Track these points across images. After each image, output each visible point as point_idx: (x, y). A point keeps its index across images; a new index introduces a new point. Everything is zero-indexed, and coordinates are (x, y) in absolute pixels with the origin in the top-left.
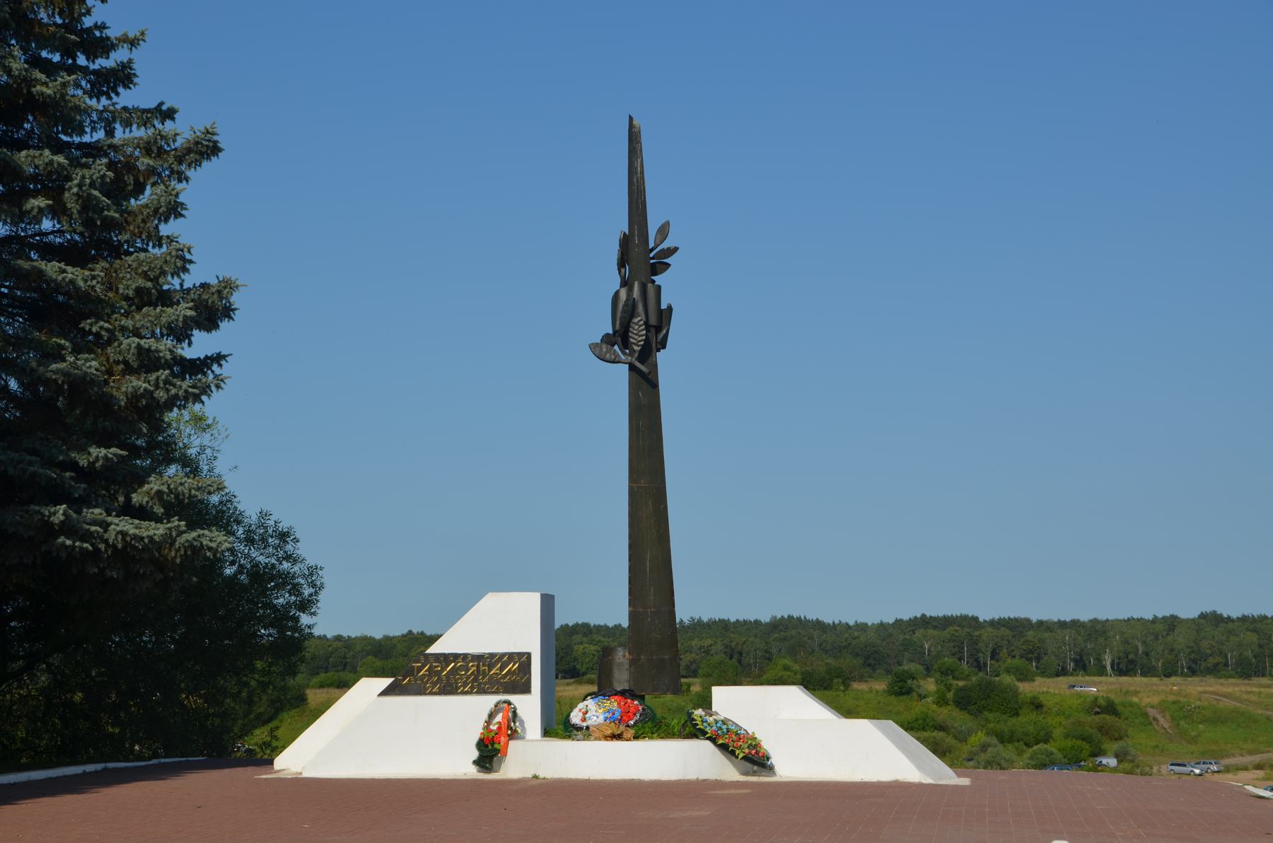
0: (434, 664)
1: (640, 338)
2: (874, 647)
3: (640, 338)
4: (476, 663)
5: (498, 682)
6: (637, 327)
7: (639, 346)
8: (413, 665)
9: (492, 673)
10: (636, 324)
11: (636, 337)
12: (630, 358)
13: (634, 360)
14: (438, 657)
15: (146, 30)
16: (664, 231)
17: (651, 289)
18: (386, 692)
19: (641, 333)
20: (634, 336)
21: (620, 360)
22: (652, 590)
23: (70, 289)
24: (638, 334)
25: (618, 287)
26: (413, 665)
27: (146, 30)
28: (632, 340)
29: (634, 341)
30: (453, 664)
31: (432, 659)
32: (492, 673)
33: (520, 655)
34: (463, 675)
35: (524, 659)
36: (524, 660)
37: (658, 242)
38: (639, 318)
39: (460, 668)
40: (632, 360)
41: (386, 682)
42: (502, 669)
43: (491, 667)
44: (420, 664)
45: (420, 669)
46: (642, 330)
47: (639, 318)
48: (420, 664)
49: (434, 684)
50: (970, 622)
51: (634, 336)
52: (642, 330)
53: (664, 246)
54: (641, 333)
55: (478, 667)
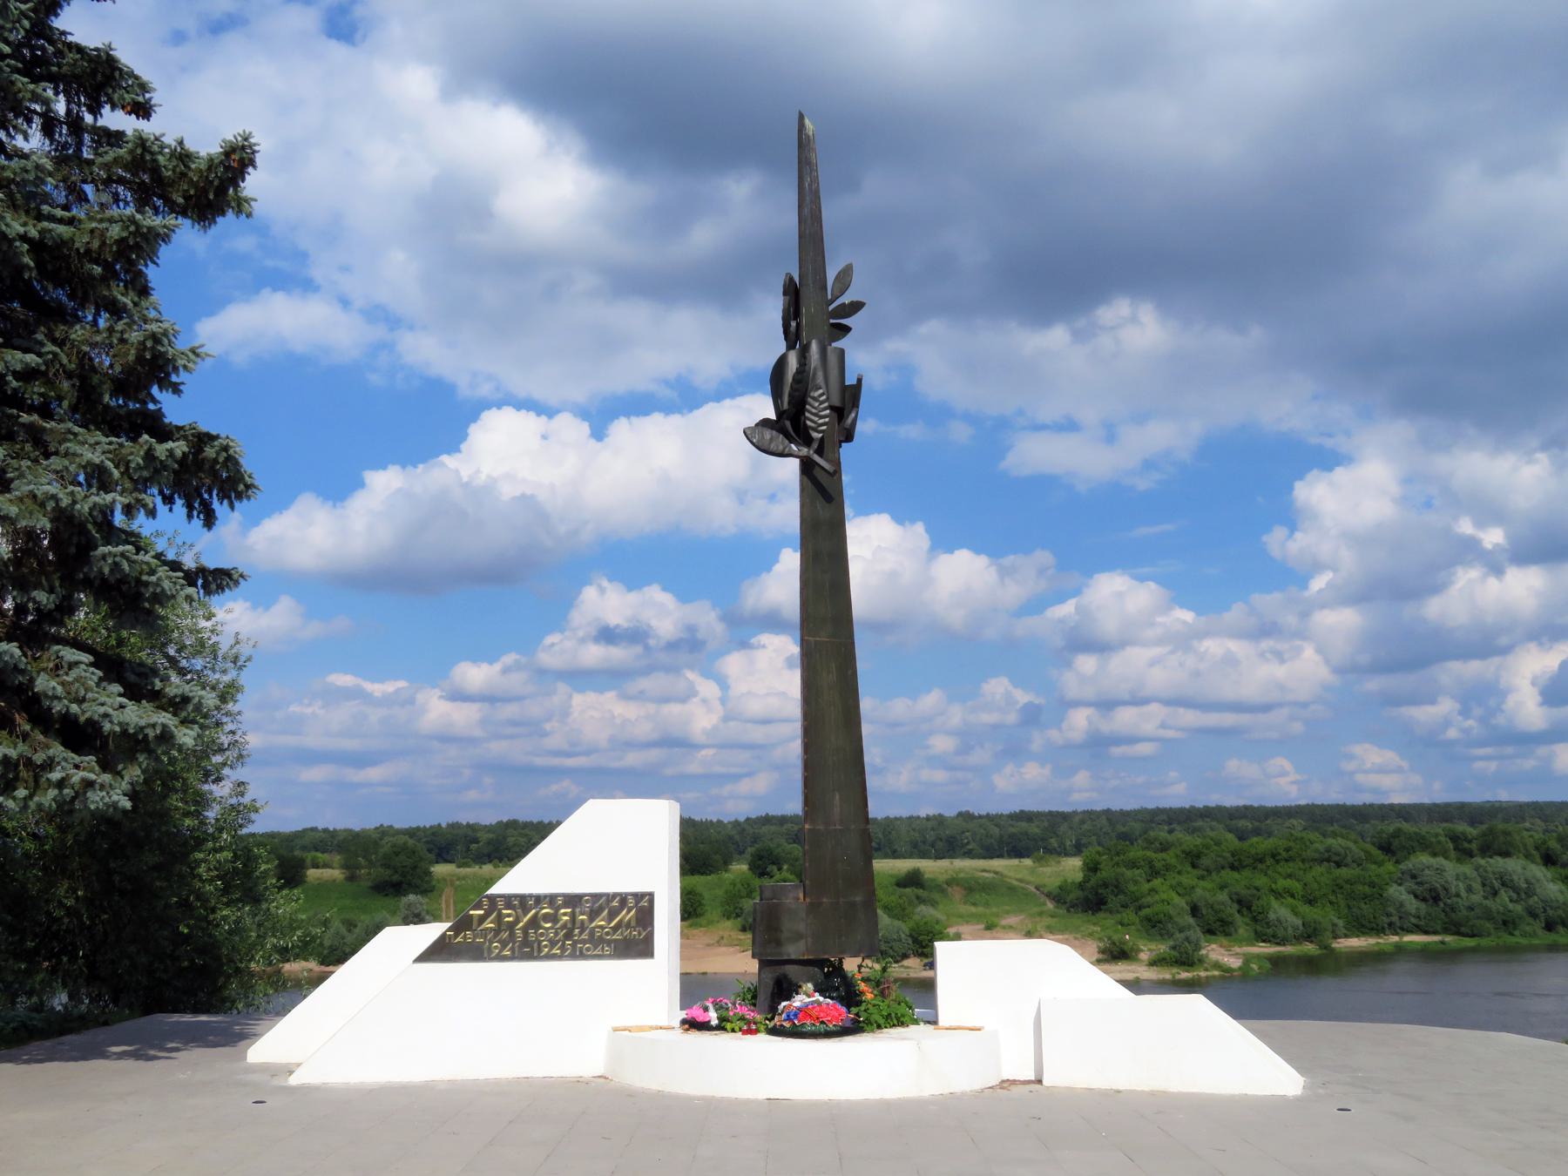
0: (504, 912)
1: (821, 421)
2: (1067, 939)
3: (821, 421)
4: (569, 910)
5: (601, 940)
6: (816, 404)
7: (819, 432)
8: (471, 912)
9: (593, 925)
10: (815, 399)
11: (816, 419)
12: (806, 450)
13: (811, 452)
14: (509, 900)
15: (171, 510)
16: (845, 277)
17: (832, 360)
18: (438, 952)
19: (823, 413)
20: (813, 417)
21: (792, 452)
22: (837, 797)
23: (87, 614)
24: (818, 417)
25: (783, 349)
26: (471, 912)
27: (171, 510)
28: (808, 423)
29: (813, 425)
30: (533, 911)
31: (500, 904)
32: (593, 925)
33: (639, 897)
34: (549, 928)
35: (627, 915)
36: (643, 906)
37: (837, 293)
38: (821, 391)
39: (546, 918)
40: (808, 452)
41: (294, 1080)
42: (610, 918)
43: (593, 914)
44: (482, 912)
45: (482, 919)
46: (825, 409)
47: (821, 391)
48: (482, 912)
49: (504, 944)
50: (1537, 802)
51: (813, 417)
52: (825, 409)
53: (846, 299)
54: (823, 413)
55: (573, 916)
